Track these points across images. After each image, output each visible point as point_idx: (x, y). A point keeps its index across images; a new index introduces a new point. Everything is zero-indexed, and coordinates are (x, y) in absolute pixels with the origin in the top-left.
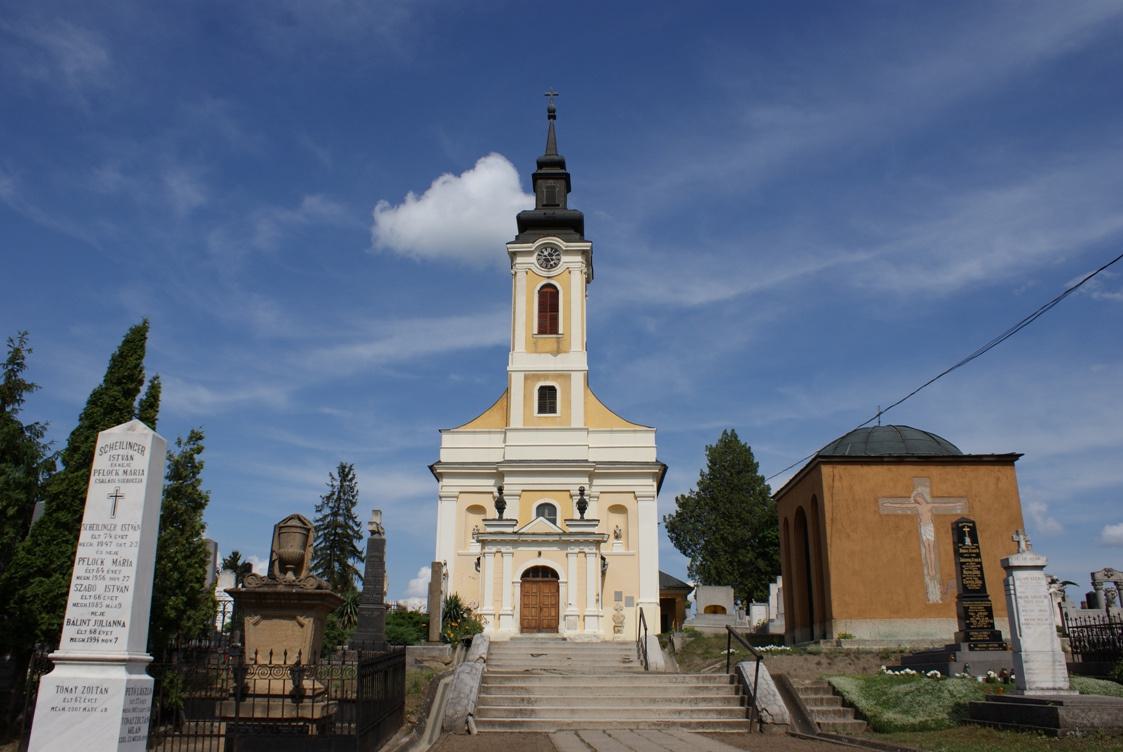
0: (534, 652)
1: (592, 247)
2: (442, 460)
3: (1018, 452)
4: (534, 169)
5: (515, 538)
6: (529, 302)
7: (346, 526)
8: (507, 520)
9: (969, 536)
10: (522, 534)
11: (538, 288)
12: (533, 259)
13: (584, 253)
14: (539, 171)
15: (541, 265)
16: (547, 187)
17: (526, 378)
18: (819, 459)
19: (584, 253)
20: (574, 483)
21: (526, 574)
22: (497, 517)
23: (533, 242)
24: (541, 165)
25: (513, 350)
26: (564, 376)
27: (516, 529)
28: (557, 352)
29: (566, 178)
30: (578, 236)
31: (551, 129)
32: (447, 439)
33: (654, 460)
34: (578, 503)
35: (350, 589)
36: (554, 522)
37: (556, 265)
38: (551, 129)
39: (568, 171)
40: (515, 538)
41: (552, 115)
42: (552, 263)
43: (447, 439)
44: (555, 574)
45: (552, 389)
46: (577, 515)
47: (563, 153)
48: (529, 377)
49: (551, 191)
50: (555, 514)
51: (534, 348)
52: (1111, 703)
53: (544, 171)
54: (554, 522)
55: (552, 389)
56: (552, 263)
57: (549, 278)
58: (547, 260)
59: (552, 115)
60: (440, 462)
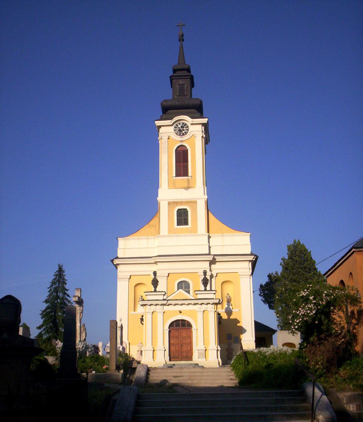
0: (176, 374)
1: (208, 121)
2: (119, 256)
3: (57, 269)
4: (171, 73)
5: (165, 302)
6: (169, 157)
7: (63, 299)
8: (159, 292)
9: (46, 313)
10: (168, 300)
11: (175, 148)
12: (172, 129)
13: (203, 124)
14: (174, 75)
15: (177, 134)
16: (179, 85)
17: (169, 204)
18: (354, 250)
19: (203, 124)
20: (149, 269)
21: (171, 325)
22: (153, 291)
23: (192, 118)
24: (175, 71)
25: (161, 187)
26: (193, 203)
27: (165, 297)
28: (187, 188)
29: (192, 78)
30: (199, 114)
31: (181, 48)
32: (122, 242)
33: (250, 253)
34: (202, 280)
35: (63, 341)
36: (188, 292)
37: (186, 133)
38: (181, 48)
39: (192, 74)
40: (165, 302)
41: (181, 39)
42: (183, 132)
43: (122, 242)
44: (189, 325)
45: (185, 211)
46: (203, 288)
47: (189, 61)
48: (171, 204)
49: (182, 87)
50: (189, 288)
51: (172, 185)
52: (154, 392)
53: (178, 73)
54: (188, 292)
55: (185, 211)
56: (183, 132)
57: (181, 141)
58: (180, 131)
59: (181, 39)
60: (117, 257)
